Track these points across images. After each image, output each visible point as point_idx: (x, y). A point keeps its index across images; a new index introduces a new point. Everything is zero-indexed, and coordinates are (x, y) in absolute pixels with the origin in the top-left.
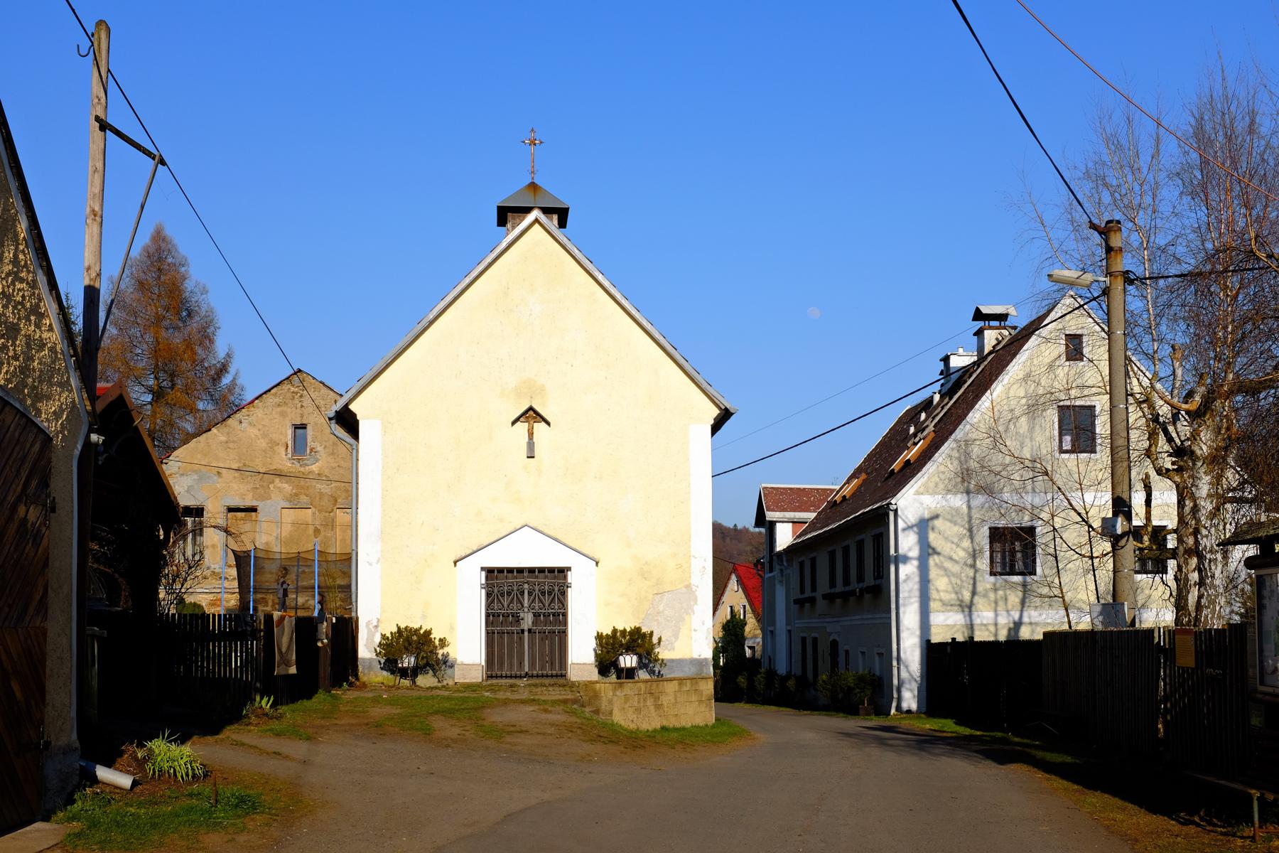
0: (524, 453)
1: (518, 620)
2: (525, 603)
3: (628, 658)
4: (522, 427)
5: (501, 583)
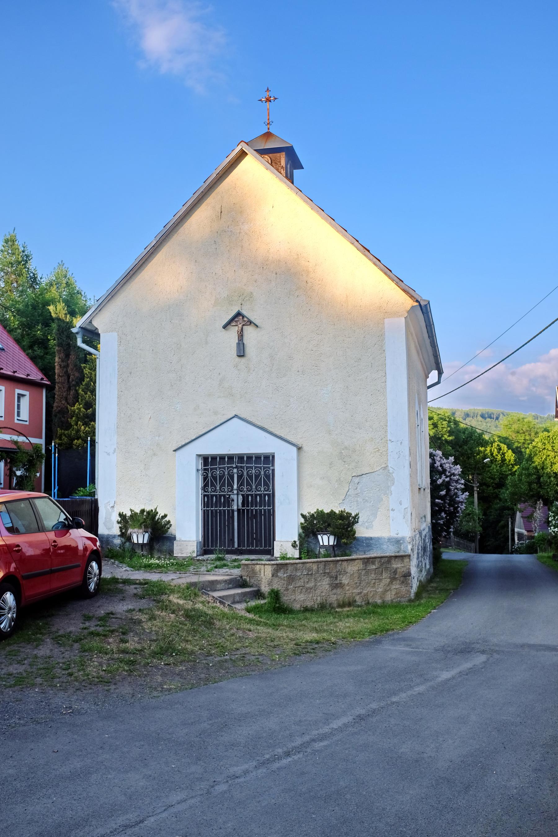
0: (234, 352)
1: (228, 501)
2: (237, 496)
3: (325, 537)
4: (233, 331)
5: (214, 468)
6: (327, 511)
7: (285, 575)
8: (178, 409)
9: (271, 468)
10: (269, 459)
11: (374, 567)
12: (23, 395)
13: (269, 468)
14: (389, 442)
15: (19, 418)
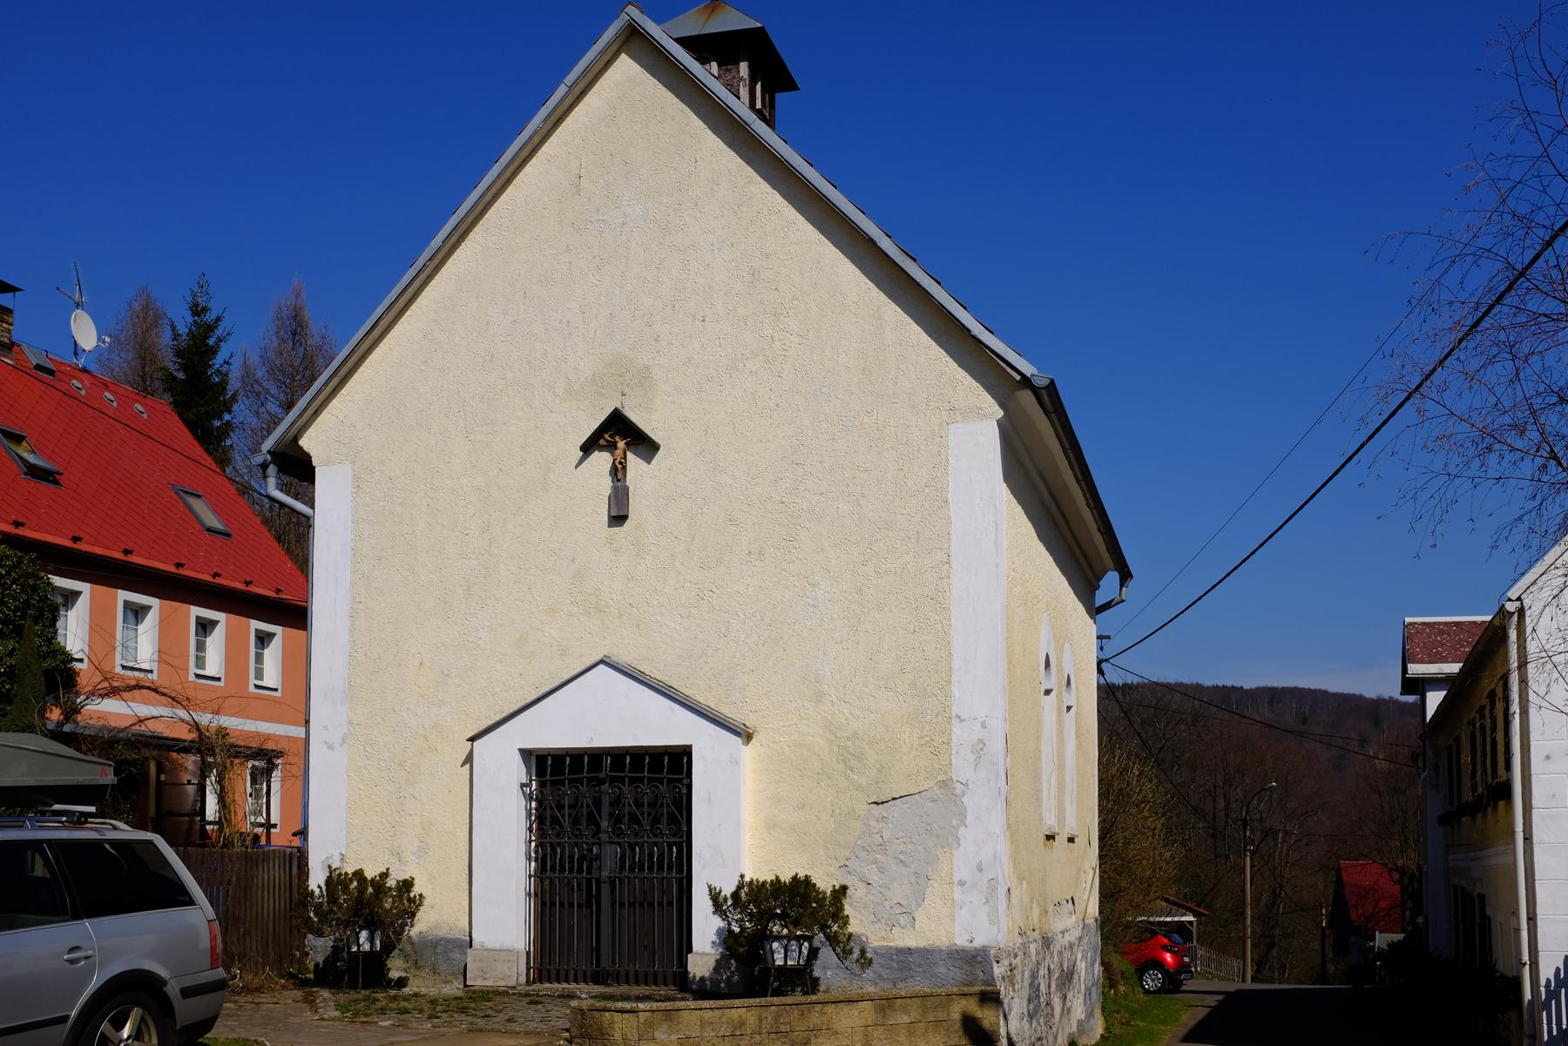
4: (601, 461)
5: (561, 778)
6: (786, 878)
7: (674, 1037)
10: (676, 761)
11: (906, 1019)
12: (271, 636)
13: (680, 781)
14: (955, 721)
15: (259, 683)
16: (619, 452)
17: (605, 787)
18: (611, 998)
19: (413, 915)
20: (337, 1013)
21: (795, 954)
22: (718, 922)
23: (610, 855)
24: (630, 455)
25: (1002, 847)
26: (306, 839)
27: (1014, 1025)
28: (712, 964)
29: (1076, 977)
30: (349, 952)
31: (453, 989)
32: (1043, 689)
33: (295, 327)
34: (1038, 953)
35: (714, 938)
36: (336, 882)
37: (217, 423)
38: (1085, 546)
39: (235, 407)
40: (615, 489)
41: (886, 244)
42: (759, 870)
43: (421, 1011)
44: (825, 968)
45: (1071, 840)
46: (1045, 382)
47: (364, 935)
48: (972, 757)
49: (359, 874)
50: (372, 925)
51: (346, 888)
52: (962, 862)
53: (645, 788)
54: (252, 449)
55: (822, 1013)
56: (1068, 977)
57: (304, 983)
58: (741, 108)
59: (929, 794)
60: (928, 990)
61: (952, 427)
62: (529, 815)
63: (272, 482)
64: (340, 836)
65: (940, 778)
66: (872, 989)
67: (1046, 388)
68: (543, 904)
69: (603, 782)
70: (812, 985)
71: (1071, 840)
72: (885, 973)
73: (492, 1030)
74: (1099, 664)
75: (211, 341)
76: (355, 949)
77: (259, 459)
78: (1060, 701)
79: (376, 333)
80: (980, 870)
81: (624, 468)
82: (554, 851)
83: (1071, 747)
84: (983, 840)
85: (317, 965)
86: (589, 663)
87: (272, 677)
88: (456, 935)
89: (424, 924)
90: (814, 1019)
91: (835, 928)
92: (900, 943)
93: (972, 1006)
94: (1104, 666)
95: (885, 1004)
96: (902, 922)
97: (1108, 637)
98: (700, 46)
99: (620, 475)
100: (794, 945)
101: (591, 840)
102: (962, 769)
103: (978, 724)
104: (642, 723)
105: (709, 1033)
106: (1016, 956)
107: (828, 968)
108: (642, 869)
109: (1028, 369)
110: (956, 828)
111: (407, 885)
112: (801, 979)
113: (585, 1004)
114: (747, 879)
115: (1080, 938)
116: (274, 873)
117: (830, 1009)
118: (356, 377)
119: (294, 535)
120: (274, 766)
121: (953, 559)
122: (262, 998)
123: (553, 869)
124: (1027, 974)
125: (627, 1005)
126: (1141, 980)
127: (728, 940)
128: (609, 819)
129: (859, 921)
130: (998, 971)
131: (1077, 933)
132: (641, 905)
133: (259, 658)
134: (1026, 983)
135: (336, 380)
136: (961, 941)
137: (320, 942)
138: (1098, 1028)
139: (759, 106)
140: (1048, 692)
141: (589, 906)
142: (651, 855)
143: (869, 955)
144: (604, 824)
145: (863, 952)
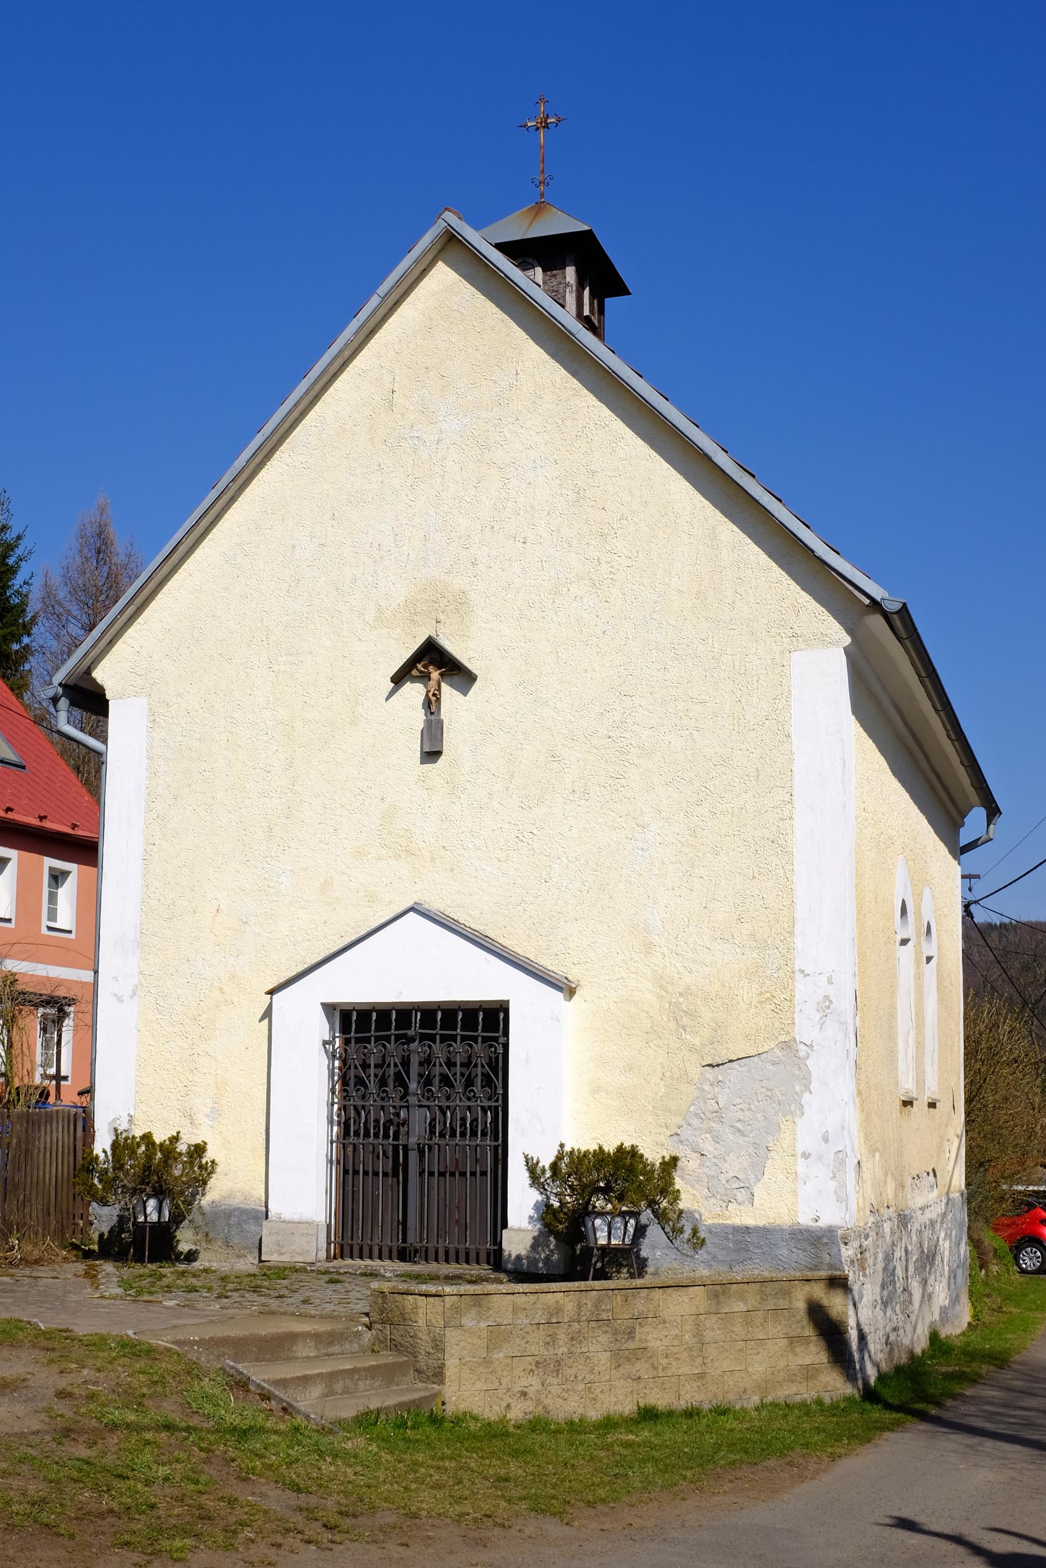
4: (414, 692)
5: (366, 1033)
6: (610, 1148)
7: (483, 1325)
8: (282, 887)
9: (502, 1040)
10: (492, 1019)
11: (742, 1307)
12: (66, 874)
13: (496, 1039)
16: (433, 684)
17: (414, 1046)
18: (417, 1277)
19: (205, 1183)
20: (120, 1291)
21: (620, 1233)
22: (535, 1196)
23: (418, 1121)
24: (445, 687)
25: (852, 1116)
26: (92, 1099)
27: (865, 1313)
28: (529, 1241)
29: (938, 1258)
30: (135, 1223)
31: (247, 1264)
32: (899, 938)
33: (100, 546)
34: (893, 1233)
35: (532, 1212)
36: (122, 1146)
37: (15, 647)
38: (948, 783)
39: (35, 630)
40: (428, 723)
41: (722, 459)
42: (583, 1139)
43: (210, 1290)
44: (654, 1247)
45: (932, 1105)
46: (897, 607)
47: (152, 1203)
48: (817, 1016)
49: (147, 1138)
50: (160, 1193)
51: (133, 1153)
52: (805, 1132)
53: (458, 1047)
54: (48, 679)
55: (648, 1299)
56: (928, 1259)
57: (88, 1255)
58: (567, 317)
59: (769, 1056)
60: (767, 1275)
61: (794, 655)
62: (332, 1075)
63: (63, 716)
64: (129, 1095)
65: (782, 1038)
66: (706, 1272)
67: (898, 612)
68: (346, 1172)
69: (411, 1040)
70: (640, 1267)
71: (932, 1105)
72: (721, 1255)
73: (284, 1313)
74: (967, 907)
75: (11, 561)
76: (141, 1219)
77: (51, 693)
78: (918, 952)
79: (175, 558)
80: (826, 1140)
81: (438, 700)
82: (359, 1114)
83: (931, 1003)
84: (830, 1109)
85: (101, 1235)
86: (399, 910)
87: (66, 918)
88: (251, 1205)
89: (217, 1191)
90: (640, 1304)
91: (664, 1204)
92: (737, 1221)
93: (819, 1292)
94: (973, 908)
95: (719, 1290)
96: (739, 1198)
97: (978, 877)
98: (521, 252)
99: (433, 708)
100: (618, 1222)
101: (398, 1103)
102: (805, 1030)
103: (824, 979)
104: (451, 976)
105: (523, 1321)
106: (867, 1237)
107: (655, 1247)
108: (453, 1134)
109: (878, 592)
110: (800, 1095)
111: (199, 1150)
112: (626, 1260)
113: (386, 1287)
114: (567, 1149)
115: (944, 1215)
116: (57, 1135)
117: (657, 1294)
118: (154, 605)
119: (89, 769)
120: (66, 1015)
121: (795, 798)
122: (42, 1271)
123: (357, 1134)
124: (880, 1256)
125: (432, 1288)
126: (1016, 1258)
127: (547, 1214)
128: (420, 1078)
129: (691, 1195)
130: (847, 1253)
131: (940, 1208)
132: (452, 1174)
133: (53, 898)
134: (880, 1265)
135: (132, 609)
136: (805, 1220)
137: (106, 1210)
138: (965, 1315)
139: (586, 312)
140: (904, 942)
141: (396, 1174)
142: (463, 1120)
143: (702, 1235)
144: (413, 1086)
145: (695, 1232)
